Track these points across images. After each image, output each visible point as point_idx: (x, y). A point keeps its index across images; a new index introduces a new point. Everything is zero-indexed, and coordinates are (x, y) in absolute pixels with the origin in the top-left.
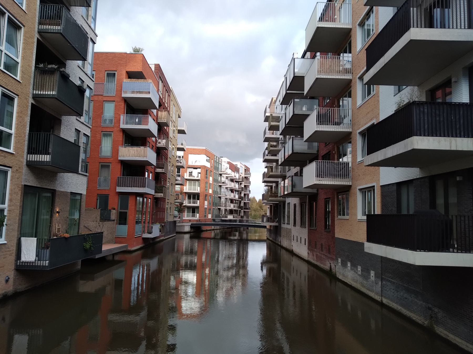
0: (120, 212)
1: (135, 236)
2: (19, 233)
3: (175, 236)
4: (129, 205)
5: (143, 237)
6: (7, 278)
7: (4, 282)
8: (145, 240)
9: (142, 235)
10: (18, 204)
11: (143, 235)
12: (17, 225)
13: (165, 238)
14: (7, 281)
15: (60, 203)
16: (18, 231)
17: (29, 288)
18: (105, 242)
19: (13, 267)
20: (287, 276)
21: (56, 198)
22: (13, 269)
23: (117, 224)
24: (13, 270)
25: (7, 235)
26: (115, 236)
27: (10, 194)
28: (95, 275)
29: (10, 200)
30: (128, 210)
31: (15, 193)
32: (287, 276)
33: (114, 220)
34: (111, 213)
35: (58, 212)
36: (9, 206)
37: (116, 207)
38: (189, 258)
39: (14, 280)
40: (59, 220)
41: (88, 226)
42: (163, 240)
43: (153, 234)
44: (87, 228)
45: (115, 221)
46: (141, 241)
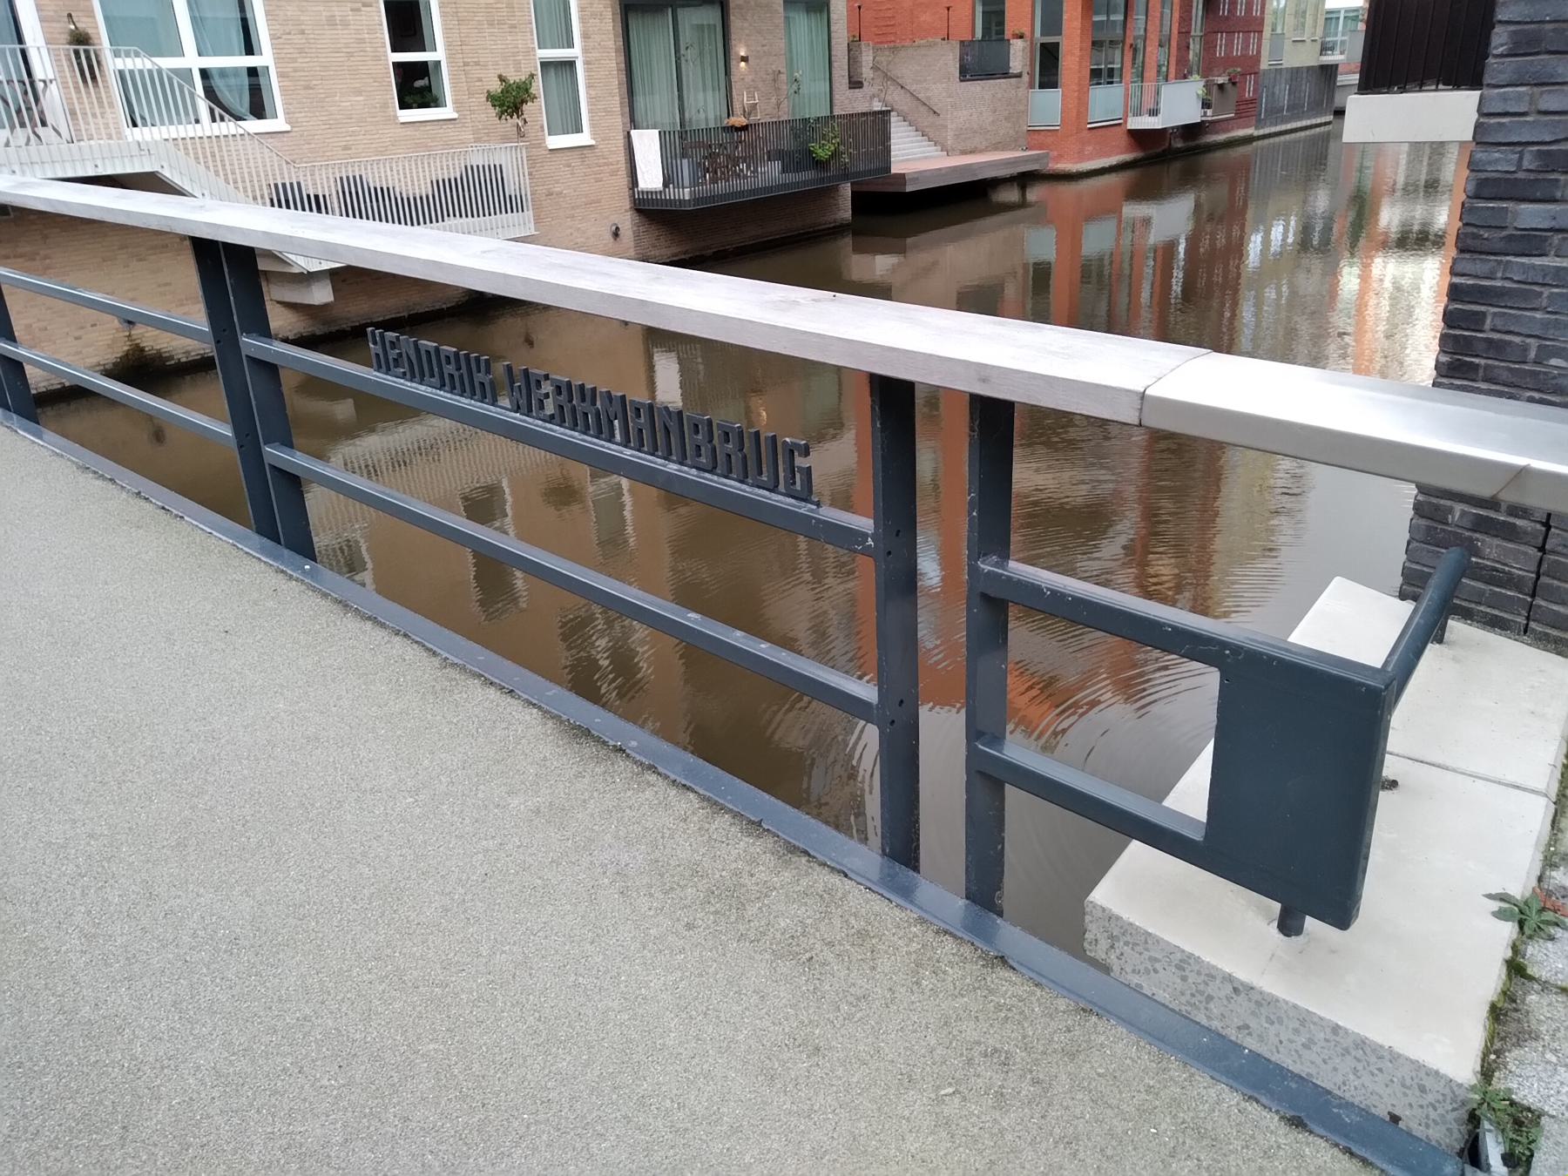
0: (1042, 45)
1: (1089, 126)
2: (628, 119)
3: (1329, 123)
4: (1065, 17)
5: (1129, 127)
6: (614, 228)
7: (609, 237)
8: (1139, 137)
9: (1126, 122)
10: (611, 44)
11: (1129, 120)
12: (618, 98)
13: (1256, 133)
14: (616, 234)
15: (747, 32)
16: (622, 115)
17: (683, 257)
18: (987, 147)
19: (627, 204)
20: (91, 368)
21: (732, 18)
22: (628, 207)
23: (1032, 86)
24: (626, 211)
25: (593, 125)
26: (1025, 128)
27: (582, 20)
28: (909, 240)
29: (585, 36)
30: (1061, 34)
31: (593, 15)
32: (91, 368)
33: (1019, 76)
34: (1012, 52)
35: (744, 59)
36: (585, 50)
37: (1026, 30)
38: (1419, 212)
39: (637, 236)
40: (753, 81)
41: (929, 98)
42: (1249, 140)
43: (1160, 116)
44: (925, 104)
45: (1026, 78)
46: (1124, 141)
